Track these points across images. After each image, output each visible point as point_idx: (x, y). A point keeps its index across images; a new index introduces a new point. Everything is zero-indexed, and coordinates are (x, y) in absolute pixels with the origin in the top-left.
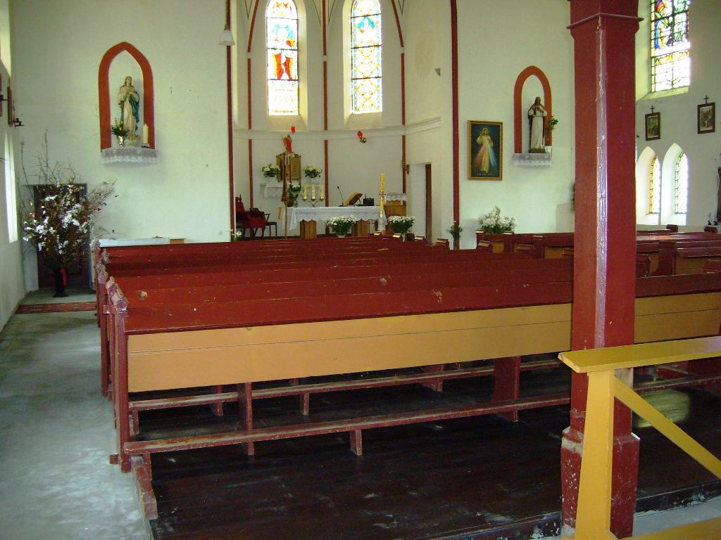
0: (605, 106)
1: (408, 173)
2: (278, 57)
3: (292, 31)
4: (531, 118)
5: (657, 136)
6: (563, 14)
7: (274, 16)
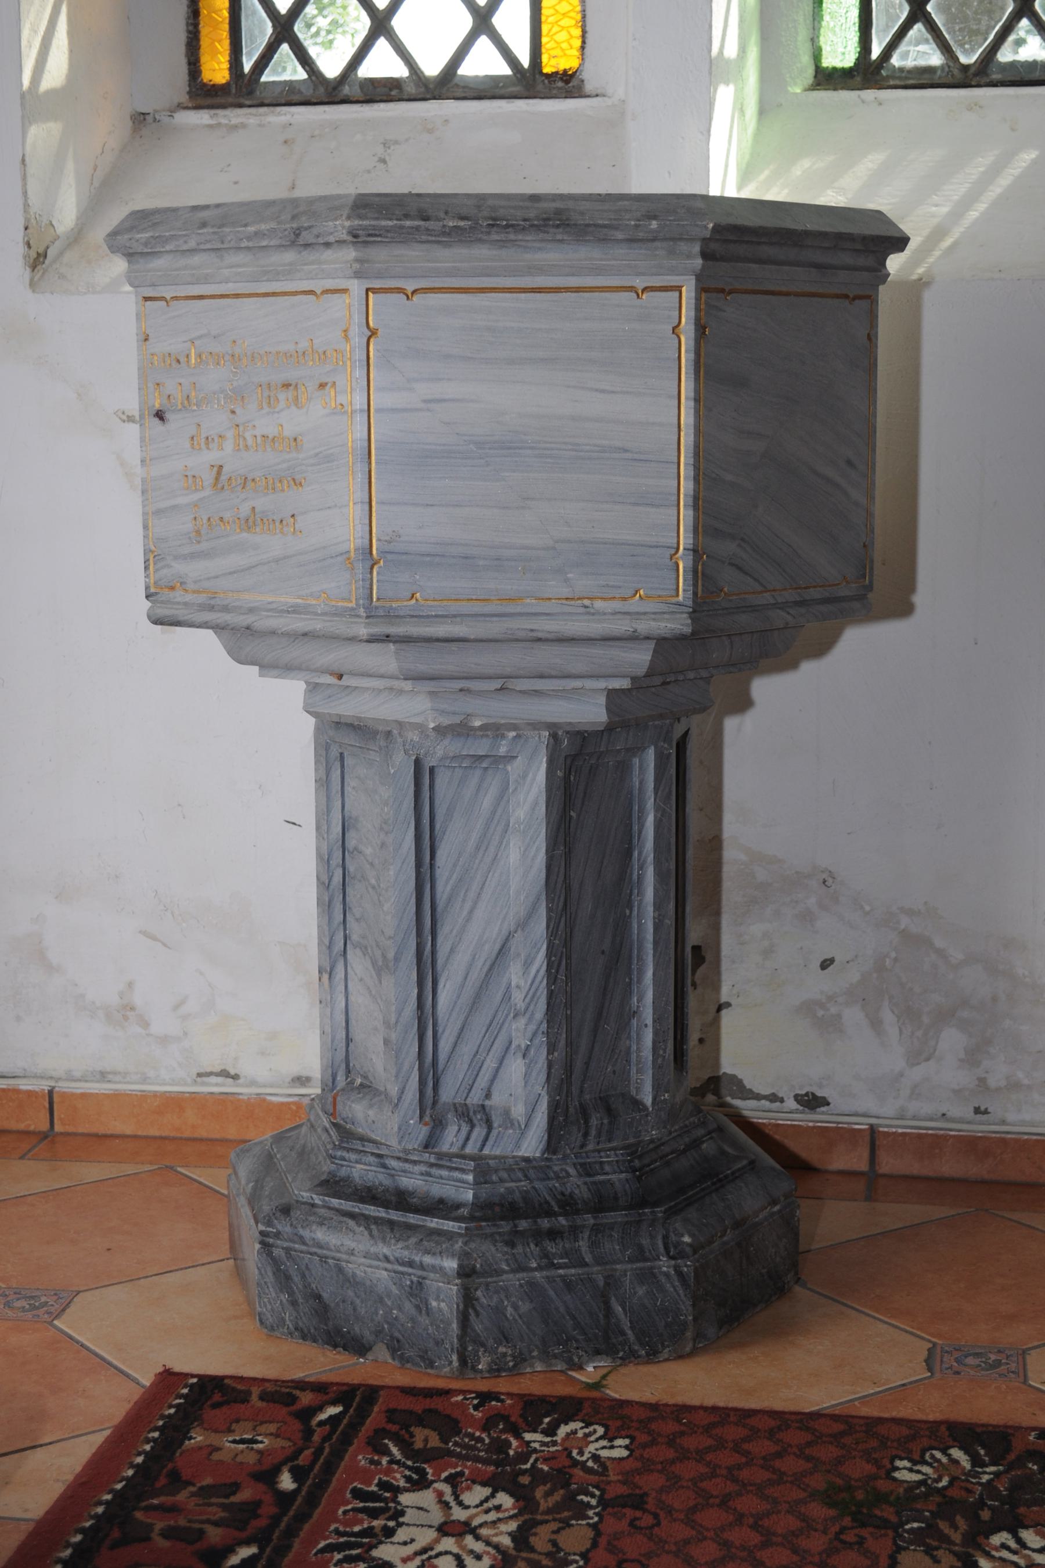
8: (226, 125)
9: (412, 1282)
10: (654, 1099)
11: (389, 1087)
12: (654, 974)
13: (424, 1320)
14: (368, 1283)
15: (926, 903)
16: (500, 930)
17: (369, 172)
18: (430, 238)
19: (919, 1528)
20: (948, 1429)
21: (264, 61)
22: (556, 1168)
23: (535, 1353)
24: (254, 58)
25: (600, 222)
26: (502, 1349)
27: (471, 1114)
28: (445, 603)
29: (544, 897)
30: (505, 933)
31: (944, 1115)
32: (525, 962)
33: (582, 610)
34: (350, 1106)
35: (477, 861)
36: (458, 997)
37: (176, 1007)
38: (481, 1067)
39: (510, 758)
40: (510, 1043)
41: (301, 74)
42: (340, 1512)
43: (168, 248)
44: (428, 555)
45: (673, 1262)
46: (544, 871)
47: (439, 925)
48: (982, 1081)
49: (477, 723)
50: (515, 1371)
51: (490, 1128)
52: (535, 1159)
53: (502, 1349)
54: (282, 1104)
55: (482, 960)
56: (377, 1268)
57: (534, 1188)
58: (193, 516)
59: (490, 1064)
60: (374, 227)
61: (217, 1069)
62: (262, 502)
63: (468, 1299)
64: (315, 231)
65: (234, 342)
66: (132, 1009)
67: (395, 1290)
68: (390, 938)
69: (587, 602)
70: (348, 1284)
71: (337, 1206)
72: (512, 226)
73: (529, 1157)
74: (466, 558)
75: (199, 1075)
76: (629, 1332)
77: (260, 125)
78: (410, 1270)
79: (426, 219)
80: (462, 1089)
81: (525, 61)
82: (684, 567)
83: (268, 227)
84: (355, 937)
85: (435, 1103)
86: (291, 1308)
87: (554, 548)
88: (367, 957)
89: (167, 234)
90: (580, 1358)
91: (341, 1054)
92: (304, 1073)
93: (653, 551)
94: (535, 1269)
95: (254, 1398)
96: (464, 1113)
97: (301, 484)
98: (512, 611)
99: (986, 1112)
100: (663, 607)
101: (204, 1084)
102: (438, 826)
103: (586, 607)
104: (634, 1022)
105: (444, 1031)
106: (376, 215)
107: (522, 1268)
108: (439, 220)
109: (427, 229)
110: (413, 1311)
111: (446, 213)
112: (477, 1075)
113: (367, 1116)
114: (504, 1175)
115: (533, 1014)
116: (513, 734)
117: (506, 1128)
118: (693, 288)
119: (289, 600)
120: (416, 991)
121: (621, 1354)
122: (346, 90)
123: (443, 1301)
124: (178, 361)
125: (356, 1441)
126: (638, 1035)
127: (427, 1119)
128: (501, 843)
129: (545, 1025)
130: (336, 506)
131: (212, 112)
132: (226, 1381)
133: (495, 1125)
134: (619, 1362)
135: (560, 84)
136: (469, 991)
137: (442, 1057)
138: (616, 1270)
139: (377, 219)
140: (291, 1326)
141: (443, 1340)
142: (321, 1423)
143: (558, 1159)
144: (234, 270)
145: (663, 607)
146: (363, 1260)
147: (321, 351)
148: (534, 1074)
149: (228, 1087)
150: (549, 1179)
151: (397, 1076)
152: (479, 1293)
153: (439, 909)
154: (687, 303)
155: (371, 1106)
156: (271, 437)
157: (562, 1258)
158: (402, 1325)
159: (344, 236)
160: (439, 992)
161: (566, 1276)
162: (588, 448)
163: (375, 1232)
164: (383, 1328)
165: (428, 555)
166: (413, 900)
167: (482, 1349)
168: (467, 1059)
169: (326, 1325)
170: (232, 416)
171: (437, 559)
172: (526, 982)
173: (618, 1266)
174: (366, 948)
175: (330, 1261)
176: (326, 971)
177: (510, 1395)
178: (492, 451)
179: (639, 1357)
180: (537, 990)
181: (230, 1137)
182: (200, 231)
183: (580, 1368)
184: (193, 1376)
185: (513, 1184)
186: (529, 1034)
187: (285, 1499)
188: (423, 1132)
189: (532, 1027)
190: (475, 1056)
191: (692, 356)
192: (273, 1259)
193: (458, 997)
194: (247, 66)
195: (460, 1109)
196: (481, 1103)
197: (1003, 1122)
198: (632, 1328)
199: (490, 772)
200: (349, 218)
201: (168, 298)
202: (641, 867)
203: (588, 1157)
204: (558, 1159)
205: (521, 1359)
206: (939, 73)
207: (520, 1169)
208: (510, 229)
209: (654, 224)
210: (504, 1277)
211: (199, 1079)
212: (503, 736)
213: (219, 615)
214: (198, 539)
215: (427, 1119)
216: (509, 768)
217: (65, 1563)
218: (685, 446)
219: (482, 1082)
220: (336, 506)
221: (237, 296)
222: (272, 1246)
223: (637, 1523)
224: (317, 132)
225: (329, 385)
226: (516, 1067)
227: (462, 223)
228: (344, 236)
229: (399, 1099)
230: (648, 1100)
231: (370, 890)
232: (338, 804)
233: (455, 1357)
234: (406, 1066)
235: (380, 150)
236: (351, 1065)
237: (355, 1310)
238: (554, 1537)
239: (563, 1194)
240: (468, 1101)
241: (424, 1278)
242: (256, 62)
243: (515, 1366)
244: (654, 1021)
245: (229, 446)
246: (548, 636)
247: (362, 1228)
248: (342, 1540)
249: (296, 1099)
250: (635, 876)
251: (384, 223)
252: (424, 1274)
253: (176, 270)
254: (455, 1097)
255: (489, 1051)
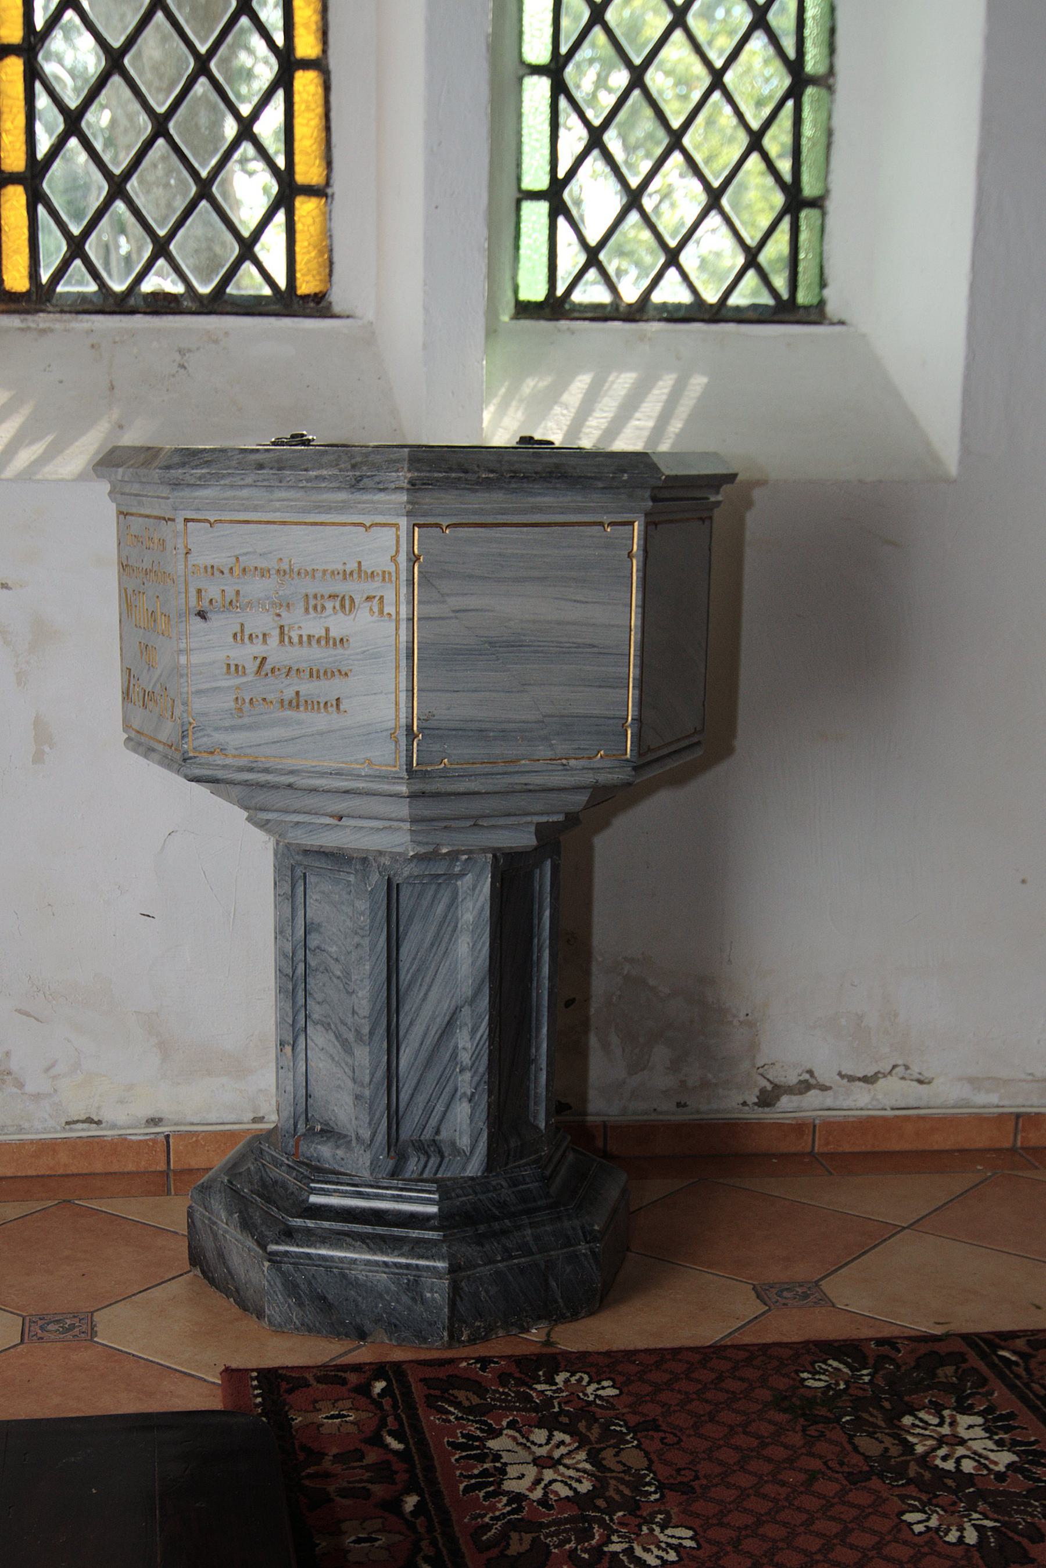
8: (36, 329)
9: (409, 1280)
10: (547, 1123)
11: (361, 1132)
12: (548, 1030)
13: (419, 1308)
14: (369, 1284)
15: (643, 953)
16: (449, 1006)
17: (174, 376)
18: (467, 486)
19: (851, 1420)
20: (815, 1345)
21: (60, 274)
22: (494, 1183)
23: (499, 1324)
24: (51, 271)
25: (589, 475)
26: (478, 1324)
27: (426, 1147)
28: (465, 766)
29: (487, 980)
30: (452, 1007)
31: (655, 1110)
32: (473, 1029)
33: (561, 768)
34: (315, 1148)
35: (432, 955)
36: (415, 1060)
37: (47, 1070)
38: (432, 1111)
39: (462, 875)
40: (456, 1090)
41: (93, 287)
42: (453, 1460)
43: (222, 482)
44: (454, 730)
45: (588, 1245)
46: (488, 960)
47: (401, 1005)
48: (683, 1083)
49: (444, 851)
50: (486, 1339)
51: (442, 1157)
52: (477, 1177)
53: (478, 1324)
54: (141, 1141)
55: (435, 1030)
56: (377, 1272)
57: (479, 1199)
58: (235, 697)
59: (440, 1108)
60: (428, 478)
61: (83, 1117)
62: (307, 688)
63: (455, 1289)
64: (377, 479)
65: (281, 559)
66: (9, 1073)
67: (393, 1288)
68: (365, 1017)
69: (564, 761)
70: (351, 1287)
71: (327, 1227)
72: (527, 477)
73: (472, 1177)
74: (481, 731)
75: (67, 1123)
76: (560, 1300)
77: (66, 330)
78: (405, 1272)
79: (466, 472)
80: (418, 1128)
81: (282, 283)
82: (632, 733)
83: (330, 473)
84: (315, 1016)
85: (397, 1140)
86: (298, 1309)
87: (543, 722)
88: (330, 1031)
89: (225, 472)
90: (528, 1323)
91: (301, 1108)
92: (157, 1115)
93: (611, 721)
94: (500, 1261)
96: (421, 1147)
97: (346, 674)
98: (512, 770)
99: (685, 1105)
100: (617, 764)
101: (71, 1130)
102: (401, 929)
103: (564, 765)
104: (533, 1067)
105: (404, 1085)
106: (428, 469)
107: (491, 1261)
108: (475, 472)
109: (466, 480)
110: (409, 1302)
111: (478, 466)
112: (429, 1117)
113: (334, 1156)
114: (460, 1192)
115: (477, 1068)
116: (465, 857)
117: (455, 1156)
118: (643, 523)
119: (333, 765)
120: (386, 1057)
121: (555, 1317)
122: (132, 301)
123: (436, 1292)
124: (222, 572)
125: (418, 1406)
126: (535, 1077)
127: (392, 1154)
128: (450, 940)
129: (487, 1076)
130: (381, 693)
131: (23, 317)
132: (280, 1372)
133: (446, 1154)
134: (553, 1323)
135: (312, 305)
136: (423, 1055)
137: (402, 1105)
138: (551, 1256)
139: (429, 471)
140: (297, 1323)
141: (435, 1322)
143: (493, 1176)
144: (285, 503)
145: (617, 764)
146: (363, 1267)
147: (369, 572)
148: (477, 1114)
149: (94, 1131)
150: (489, 1191)
151: (370, 1124)
152: (463, 1284)
153: (401, 993)
154: (638, 534)
155: (338, 1147)
156: (317, 636)
157: (517, 1251)
158: (399, 1314)
159: (405, 485)
160: (400, 1056)
161: (519, 1264)
162: (568, 645)
163: (372, 1245)
164: (382, 1316)
165: (454, 730)
166: (385, 987)
167: (464, 1325)
168: (421, 1106)
169: (330, 1319)
170: (277, 618)
171: (460, 732)
172: (472, 1045)
173: (552, 1253)
174: (329, 1024)
175: (335, 1270)
176: (289, 1044)
177: (501, 1357)
178: (501, 649)
179: (566, 1318)
180: (481, 1050)
181: (97, 1171)
182: (259, 472)
183: (528, 1331)
184: (253, 1370)
185: (464, 1199)
186: (474, 1084)
188: (390, 1164)
189: (476, 1078)
190: (428, 1103)
191: (641, 574)
192: (282, 1273)
193: (415, 1060)
194: (45, 277)
195: (416, 1144)
196: (432, 1138)
197: (698, 1112)
198: (562, 1298)
199: (444, 886)
200: (409, 471)
201: (212, 521)
202: (540, 950)
203: (513, 1172)
204: (493, 1176)
205: (490, 1329)
206: (609, 309)
207: (469, 1186)
208: (525, 480)
209: (625, 477)
210: (478, 1269)
211: (67, 1127)
212: (458, 860)
213: (260, 775)
214: (241, 715)
215: (392, 1154)
216: (459, 883)
218: (635, 642)
219: (433, 1122)
220: (381, 693)
221: (284, 523)
222: (280, 1262)
223: (665, 1441)
224: (117, 339)
225: (377, 598)
226: (462, 1111)
227: (491, 475)
228: (405, 485)
229: (371, 1141)
230: (542, 1125)
231: (335, 980)
232: (301, 913)
233: (445, 1334)
234: (378, 1114)
235: (178, 357)
236: (309, 1115)
237: (357, 1306)
238: (618, 1459)
239: (499, 1202)
240: (422, 1138)
241: (419, 1277)
242: (52, 275)
243: (485, 1335)
244: (547, 1066)
245: (274, 640)
246: (537, 788)
247: (359, 1243)
248: (473, 1481)
249: (152, 1136)
250: (535, 957)
251: (436, 475)
252: (419, 1273)
253: (225, 499)
254: (412, 1135)
255: (439, 1098)
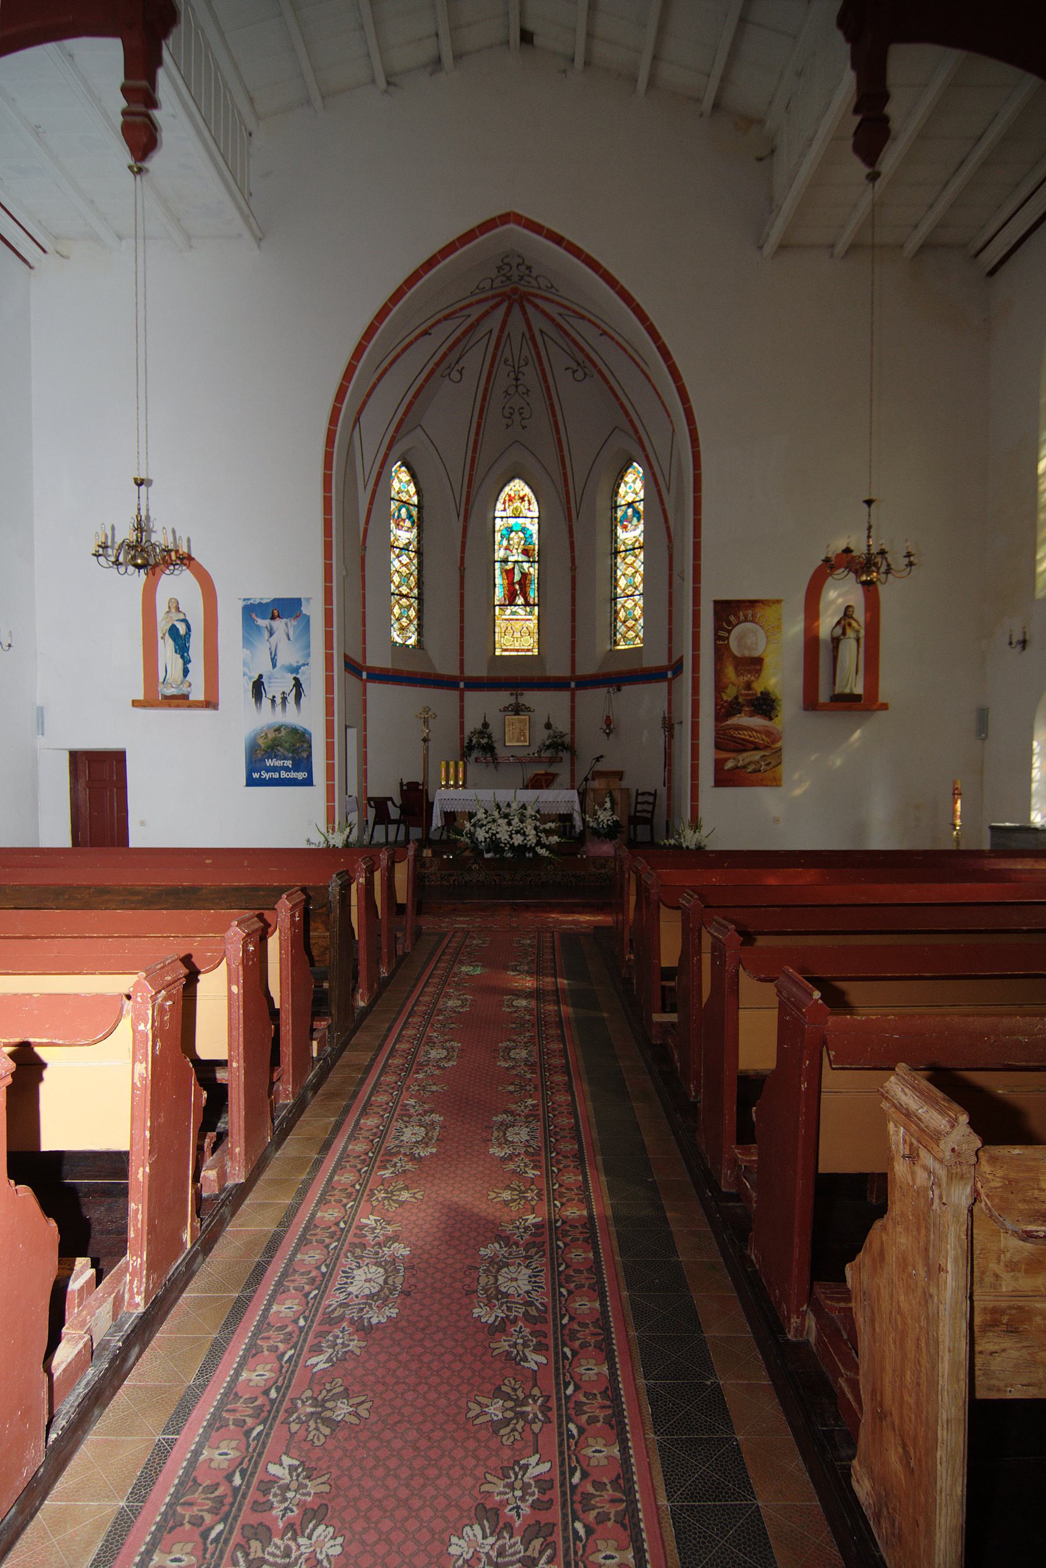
0: (857, 1325)
1: (664, 718)
2: (510, 573)
3: (531, 535)
4: (836, 641)
5: (301, 775)
6: (838, 5)
7: (504, 514)
95: (291, 1289)
142: (312, 1299)
187: (342, 1230)
217: (137, 1565)
